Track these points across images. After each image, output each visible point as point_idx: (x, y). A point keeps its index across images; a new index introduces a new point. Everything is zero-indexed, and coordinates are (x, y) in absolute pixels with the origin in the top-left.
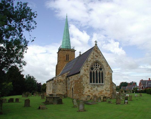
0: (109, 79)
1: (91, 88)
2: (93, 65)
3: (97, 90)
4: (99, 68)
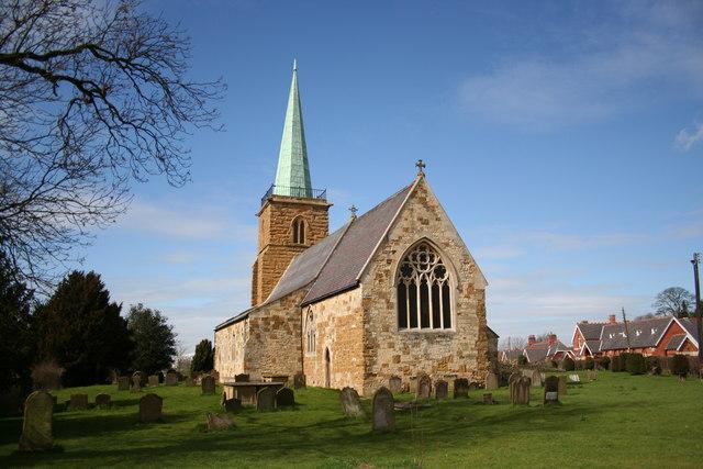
0: (474, 311)
1: (402, 346)
2: (410, 257)
3: (427, 356)
4: (431, 266)
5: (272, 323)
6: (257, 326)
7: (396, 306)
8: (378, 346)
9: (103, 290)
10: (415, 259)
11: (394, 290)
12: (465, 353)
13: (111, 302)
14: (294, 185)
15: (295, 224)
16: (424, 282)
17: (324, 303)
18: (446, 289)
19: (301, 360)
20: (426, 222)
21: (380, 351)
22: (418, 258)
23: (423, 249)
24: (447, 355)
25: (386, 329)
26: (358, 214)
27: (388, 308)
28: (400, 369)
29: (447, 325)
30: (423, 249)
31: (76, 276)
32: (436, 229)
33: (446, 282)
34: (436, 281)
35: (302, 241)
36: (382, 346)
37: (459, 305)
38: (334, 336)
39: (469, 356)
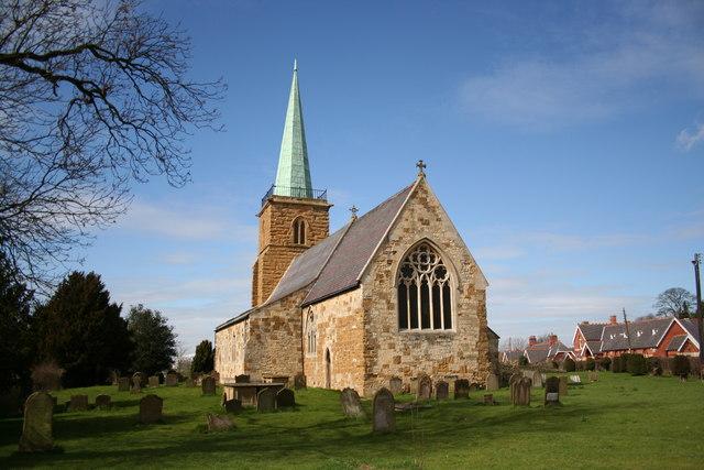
0: (475, 312)
1: (402, 346)
2: (411, 258)
3: (427, 356)
4: (432, 267)
5: (273, 324)
6: (258, 327)
7: (396, 307)
8: (379, 347)
9: (103, 290)
10: (415, 259)
11: (395, 291)
12: (466, 354)
13: (111, 303)
14: (294, 185)
15: (296, 225)
16: (424, 282)
17: (324, 303)
18: (447, 289)
19: (302, 360)
20: (426, 223)
21: (380, 352)
22: (419, 259)
23: (423, 249)
24: (448, 355)
25: (387, 330)
26: (359, 215)
27: (388, 308)
28: (401, 370)
29: (448, 325)
30: (423, 249)
31: (76, 277)
32: (437, 229)
33: (446, 283)
34: (436, 282)
35: (302, 242)
36: (382, 347)
37: (459, 306)
38: (335, 337)
39: (470, 357)
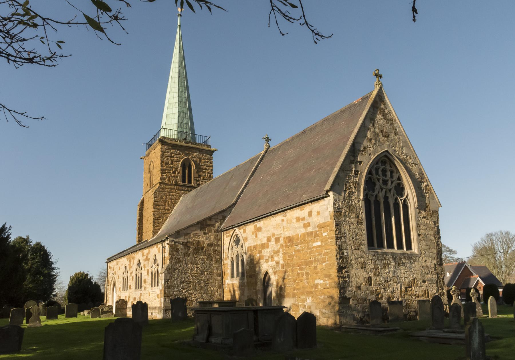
1: (372, 266)
2: (374, 171)
3: (396, 278)
6: (177, 251)
7: (364, 222)
8: (351, 265)
11: (362, 204)
14: (180, 129)
15: (183, 165)
16: (386, 198)
17: (259, 224)
21: (353, 272)
22: (380, 172)
23: (384, 163)
26: (273, 144)
28: (372, 293)
29: (409, 247)
30: (384, 163)
33: (405, 200)
34: (396, 199)
35: (190, 182)
36: (355, 267)
37: (418, 226)
38: (280, 258)
